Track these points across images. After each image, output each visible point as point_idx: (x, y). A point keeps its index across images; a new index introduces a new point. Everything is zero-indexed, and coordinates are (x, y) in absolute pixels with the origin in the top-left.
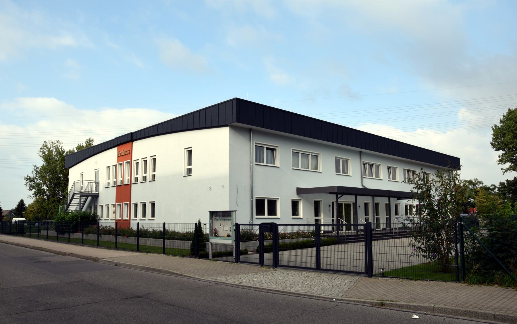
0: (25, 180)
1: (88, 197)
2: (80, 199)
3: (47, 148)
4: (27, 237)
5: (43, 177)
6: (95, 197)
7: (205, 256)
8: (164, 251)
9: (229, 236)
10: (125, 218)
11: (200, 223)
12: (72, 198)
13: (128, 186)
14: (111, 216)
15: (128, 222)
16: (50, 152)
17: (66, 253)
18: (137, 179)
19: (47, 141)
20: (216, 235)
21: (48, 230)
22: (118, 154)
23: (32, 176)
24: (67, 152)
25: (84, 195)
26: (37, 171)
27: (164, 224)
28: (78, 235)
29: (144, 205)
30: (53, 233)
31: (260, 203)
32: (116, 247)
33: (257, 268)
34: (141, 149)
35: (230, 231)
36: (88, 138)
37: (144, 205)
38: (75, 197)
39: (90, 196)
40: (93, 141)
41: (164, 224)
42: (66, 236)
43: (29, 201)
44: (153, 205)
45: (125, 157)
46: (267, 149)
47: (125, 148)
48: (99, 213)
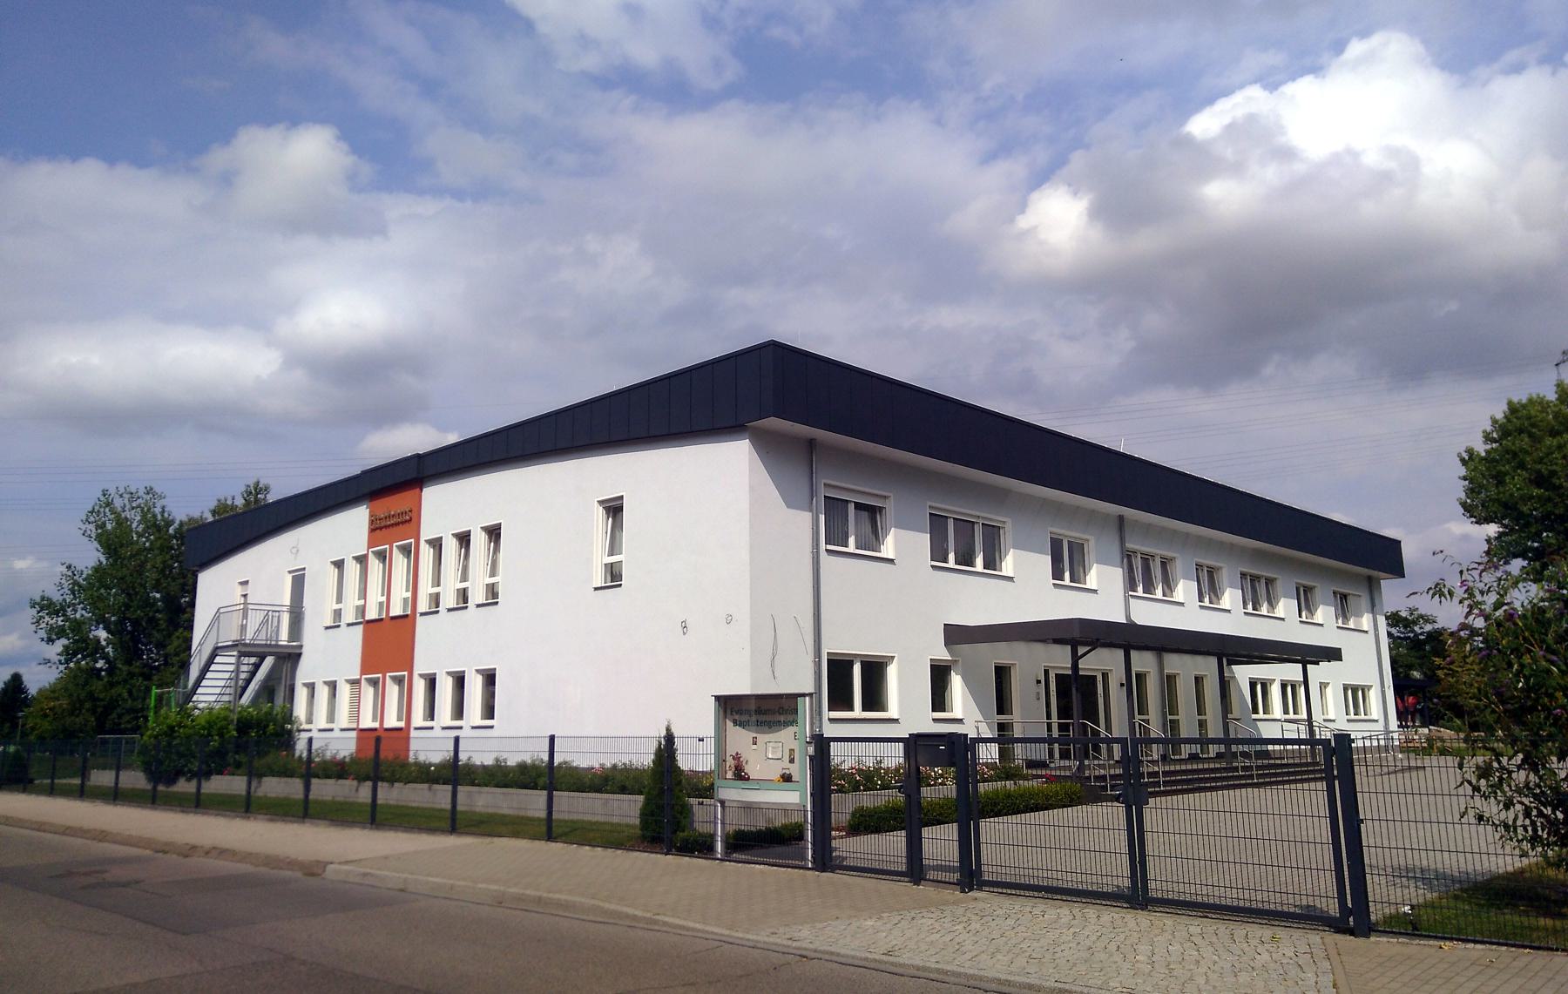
0: (34, 611)
1: (262, 659)
2: (238, 664)
3: (113, 512)
4: (41, 791)
5: (95, 603)
6: (290, 658)
7: (700, 847)
8: (550, 830)
9: (787, 778)
10: (392, 721)
11: (670, 738)
12: (210, 661)
13: (406, 622)
14: (343, 719)
15: (401, 735)
16: (121, 522)
17: (194, 847)
18: (436, 599)
19: (112, 491)
20: (740, 775)
21: (118, 770)
22: (372, 522)
23: (56, 597)
24: (182, 524)
25: (251, 652)
26: (75, 583)
27: (552, 738)
28: (230, 784)
29: (460, 681)
30: (134, 779)
31: (839, 669)
32: (376, 817)
33: (905, 887)
34: (445, 506)
35: (792, 761)
36: (251, 482)
37: (460, 681)
38: (218, 659)
39: (271, 654)
40: (267, 489)
41: (552, 738)
42: (184, 786)
43: (38, 679)
44: (490, 678)
45: (397, 528)
46: (858, 506)
47: (394, 504)
48: (300, 710)
